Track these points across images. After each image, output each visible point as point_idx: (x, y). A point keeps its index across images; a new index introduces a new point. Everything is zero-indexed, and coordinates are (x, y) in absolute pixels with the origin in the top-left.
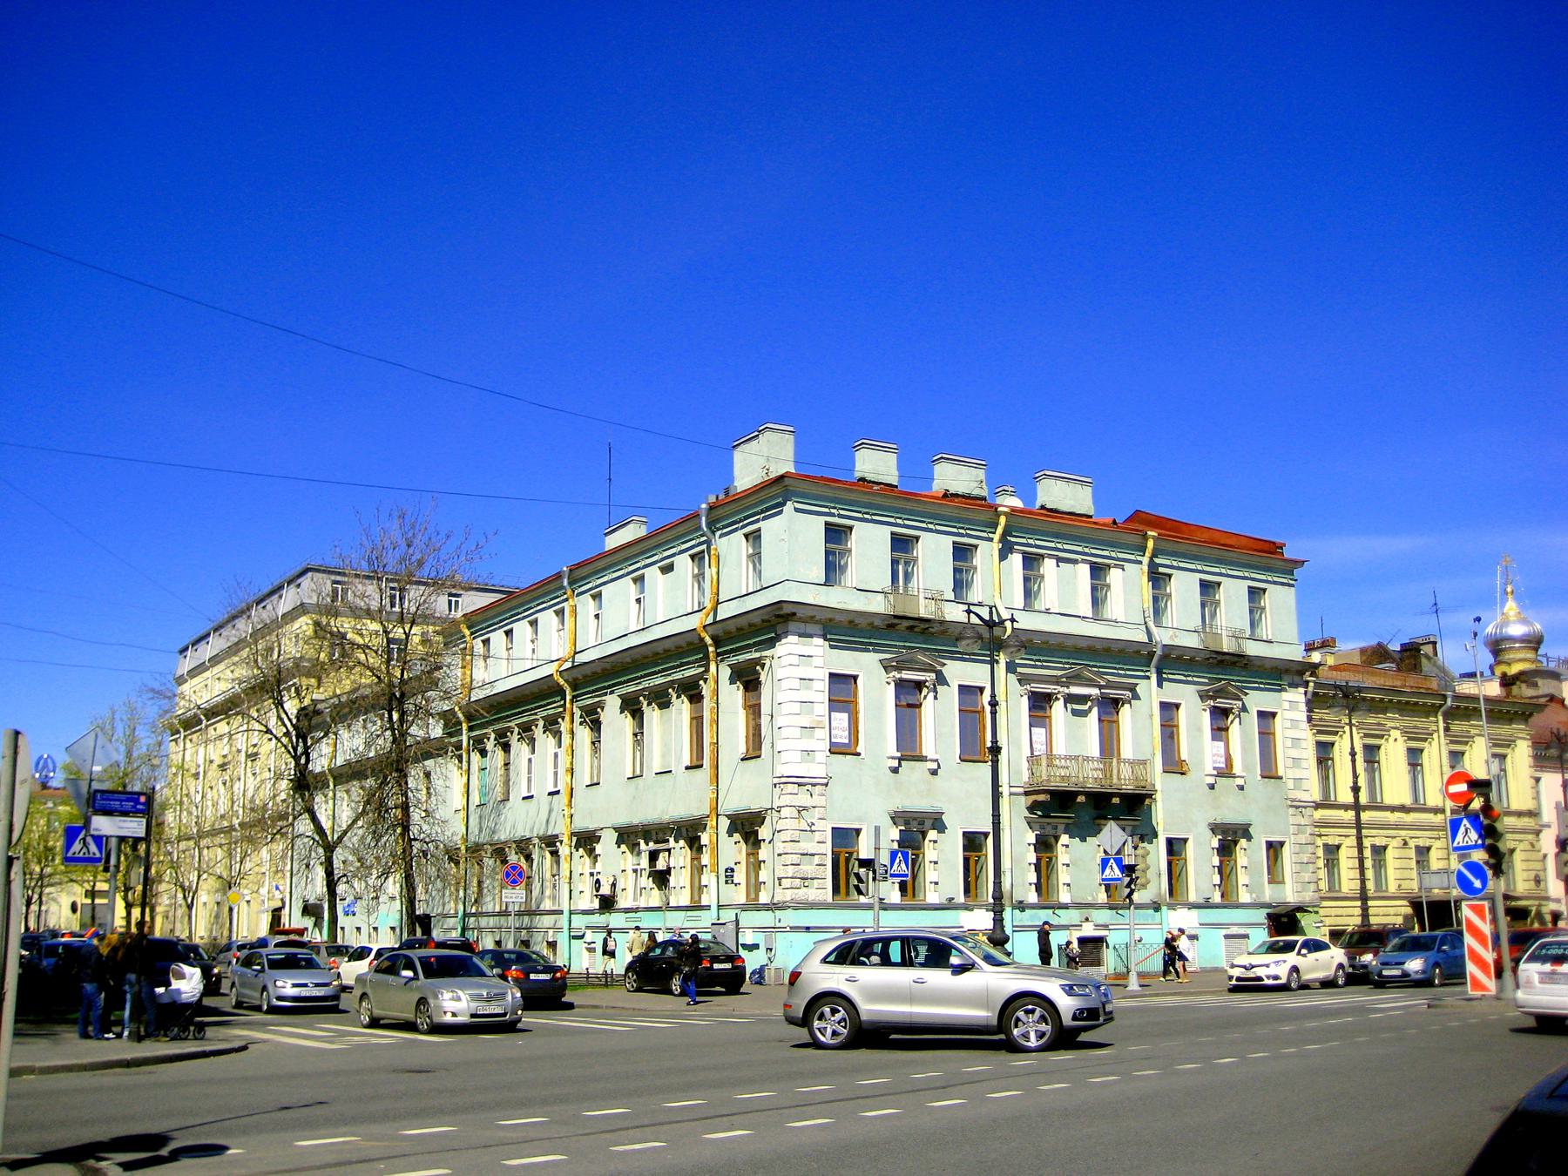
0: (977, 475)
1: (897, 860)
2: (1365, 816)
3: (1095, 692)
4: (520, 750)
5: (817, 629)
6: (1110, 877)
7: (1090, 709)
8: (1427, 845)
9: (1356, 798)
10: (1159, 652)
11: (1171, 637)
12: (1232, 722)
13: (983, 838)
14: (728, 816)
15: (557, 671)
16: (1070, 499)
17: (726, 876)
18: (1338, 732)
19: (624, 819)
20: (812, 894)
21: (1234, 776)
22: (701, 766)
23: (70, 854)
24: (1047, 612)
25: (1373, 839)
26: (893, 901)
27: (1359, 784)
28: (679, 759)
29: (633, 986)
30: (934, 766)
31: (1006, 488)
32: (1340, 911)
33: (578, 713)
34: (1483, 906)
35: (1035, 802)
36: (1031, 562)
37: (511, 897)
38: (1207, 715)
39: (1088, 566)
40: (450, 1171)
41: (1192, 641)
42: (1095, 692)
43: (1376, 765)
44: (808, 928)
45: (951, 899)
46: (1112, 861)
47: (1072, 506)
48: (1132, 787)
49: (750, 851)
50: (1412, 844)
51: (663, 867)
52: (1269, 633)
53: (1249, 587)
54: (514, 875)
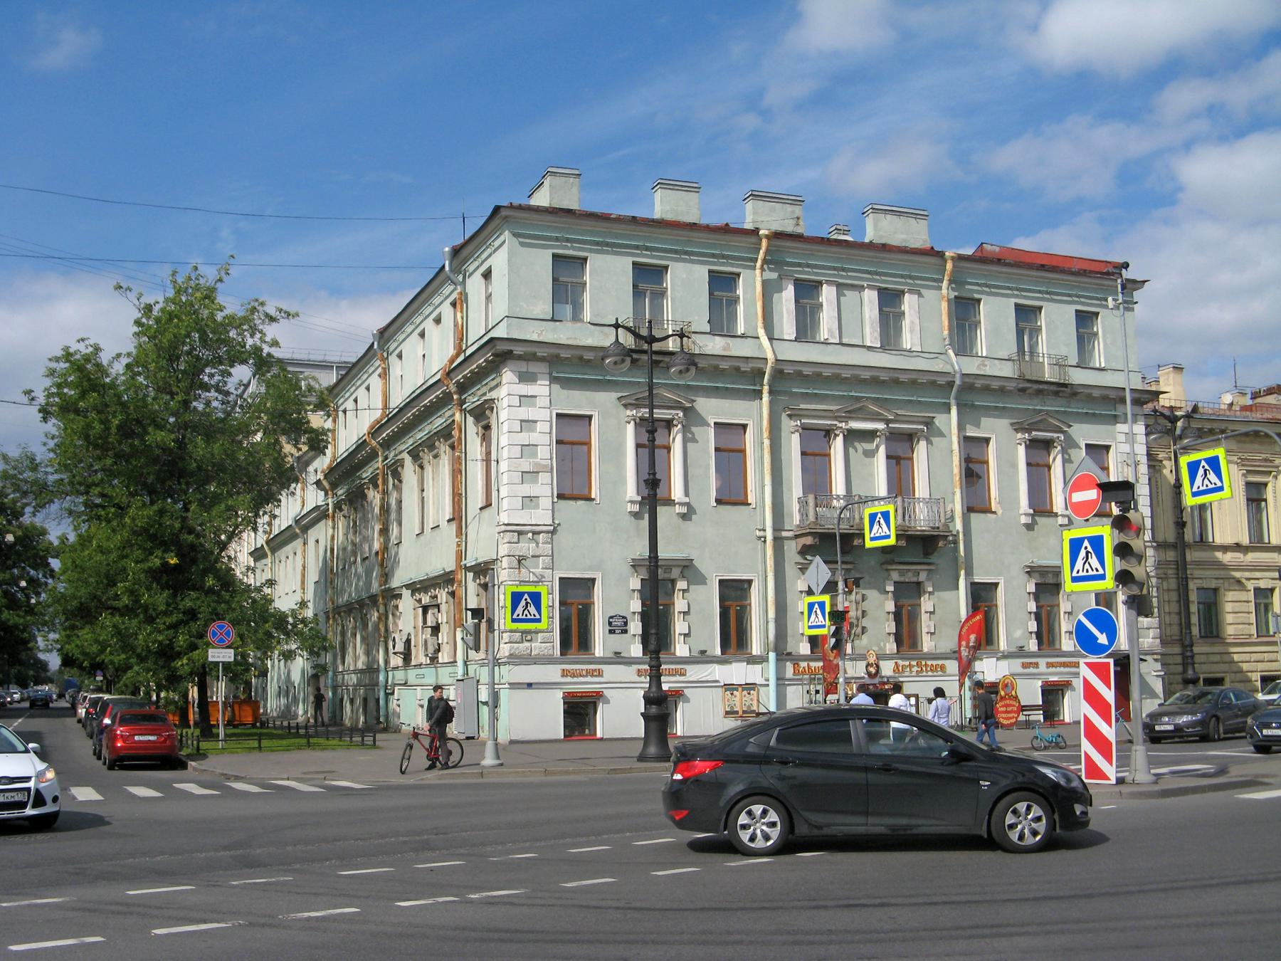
0: (793, 212)
2: (1191, 556)
3: (880, 426)
5: (542, 368)
6: (815, 624)
7: (878, 447)
8: (1213, 587)
9: (1181, 535)
10: (958, 382)
11: (978, 366)
12: (1054, 459)
13: (746, 586)
16: (902, 233)
18: (1271, 472)
20: (537, 647)
21: (1056, 515)
23: (515, 617)
24: (826, 343)
25: (1200, 581)
26: (802, 652)
27: (1184, 519)
28: (444, 516)
30: (684, 510)
31: (838, 227)
32: (1254, 657)
33: (390, 473)
34: (1109, 663)
35: (804, 546)
36: (807, 291)
37: (219, 657)
38: (1021, 450)
39: (876, 293)
40: (103, 939)
41: (1007, 370)
42: (880, 426)
43: (1263, 503)
44: (530, 685)
45: (703, 652)
47: (905, 241)
48: (927, 529)
50: (1250, 585)
51: (432, 622)
52: (1102, 360)
53: (1077, 311)
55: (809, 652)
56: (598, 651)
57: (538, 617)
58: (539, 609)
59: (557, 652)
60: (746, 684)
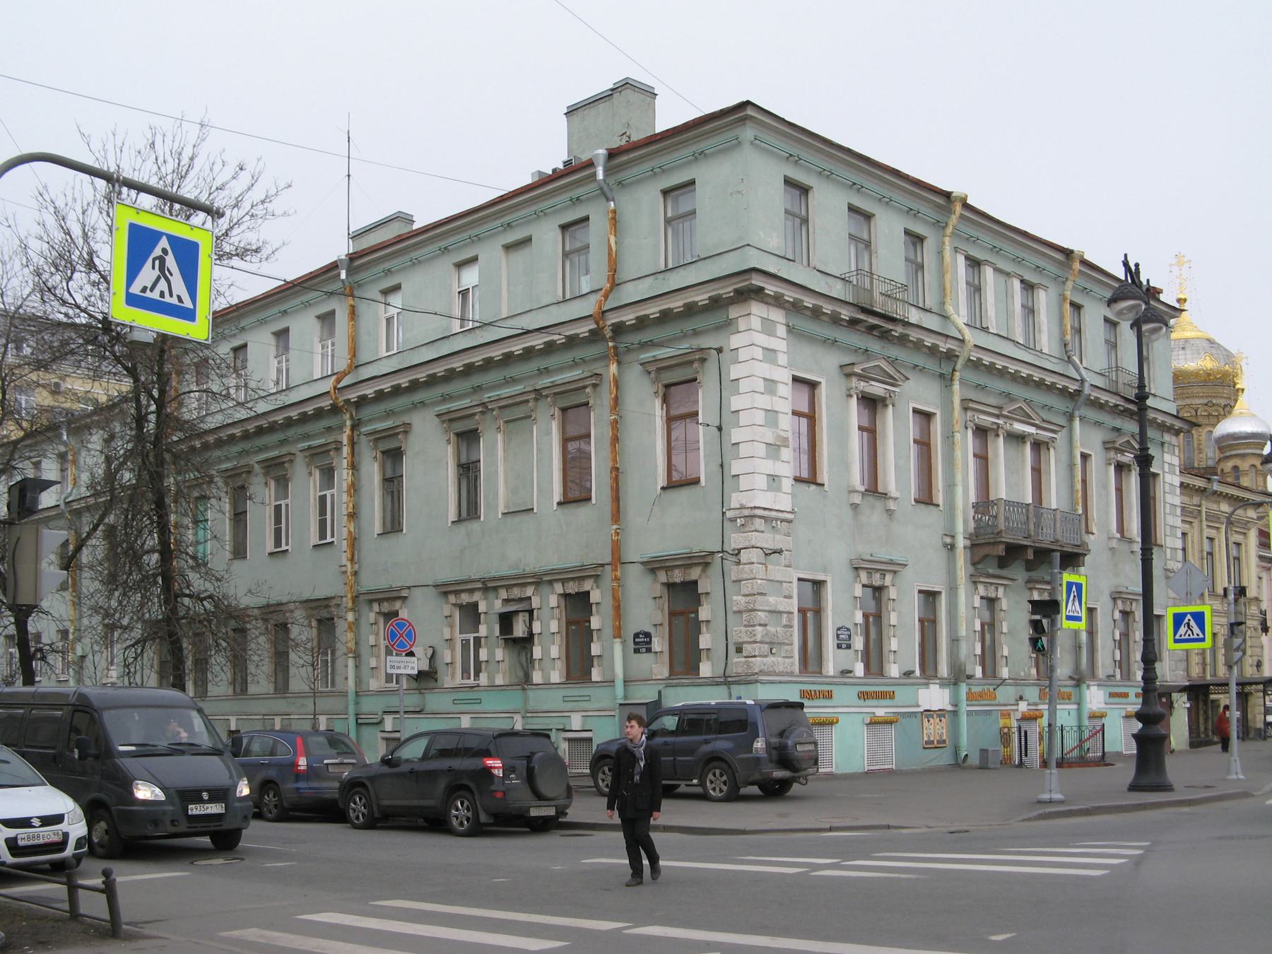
1: (1072, 595)
4: (263, 493)
14: (653, 566)
15: (335, 388)
17: (635, 643)
19: (447, 574)
22: (589, 499)
23: (1177, 637)
28: (545, 491)
29: (721, 791)
46: (1189, 617)
49: (680, 607)
51: (524, 633)
54: (401, 635)
55: (862, 675)
56: (830, 668)
57: (1201, 636)
58: (1202, 629)
59: (797, 670)
60: (940, 710)
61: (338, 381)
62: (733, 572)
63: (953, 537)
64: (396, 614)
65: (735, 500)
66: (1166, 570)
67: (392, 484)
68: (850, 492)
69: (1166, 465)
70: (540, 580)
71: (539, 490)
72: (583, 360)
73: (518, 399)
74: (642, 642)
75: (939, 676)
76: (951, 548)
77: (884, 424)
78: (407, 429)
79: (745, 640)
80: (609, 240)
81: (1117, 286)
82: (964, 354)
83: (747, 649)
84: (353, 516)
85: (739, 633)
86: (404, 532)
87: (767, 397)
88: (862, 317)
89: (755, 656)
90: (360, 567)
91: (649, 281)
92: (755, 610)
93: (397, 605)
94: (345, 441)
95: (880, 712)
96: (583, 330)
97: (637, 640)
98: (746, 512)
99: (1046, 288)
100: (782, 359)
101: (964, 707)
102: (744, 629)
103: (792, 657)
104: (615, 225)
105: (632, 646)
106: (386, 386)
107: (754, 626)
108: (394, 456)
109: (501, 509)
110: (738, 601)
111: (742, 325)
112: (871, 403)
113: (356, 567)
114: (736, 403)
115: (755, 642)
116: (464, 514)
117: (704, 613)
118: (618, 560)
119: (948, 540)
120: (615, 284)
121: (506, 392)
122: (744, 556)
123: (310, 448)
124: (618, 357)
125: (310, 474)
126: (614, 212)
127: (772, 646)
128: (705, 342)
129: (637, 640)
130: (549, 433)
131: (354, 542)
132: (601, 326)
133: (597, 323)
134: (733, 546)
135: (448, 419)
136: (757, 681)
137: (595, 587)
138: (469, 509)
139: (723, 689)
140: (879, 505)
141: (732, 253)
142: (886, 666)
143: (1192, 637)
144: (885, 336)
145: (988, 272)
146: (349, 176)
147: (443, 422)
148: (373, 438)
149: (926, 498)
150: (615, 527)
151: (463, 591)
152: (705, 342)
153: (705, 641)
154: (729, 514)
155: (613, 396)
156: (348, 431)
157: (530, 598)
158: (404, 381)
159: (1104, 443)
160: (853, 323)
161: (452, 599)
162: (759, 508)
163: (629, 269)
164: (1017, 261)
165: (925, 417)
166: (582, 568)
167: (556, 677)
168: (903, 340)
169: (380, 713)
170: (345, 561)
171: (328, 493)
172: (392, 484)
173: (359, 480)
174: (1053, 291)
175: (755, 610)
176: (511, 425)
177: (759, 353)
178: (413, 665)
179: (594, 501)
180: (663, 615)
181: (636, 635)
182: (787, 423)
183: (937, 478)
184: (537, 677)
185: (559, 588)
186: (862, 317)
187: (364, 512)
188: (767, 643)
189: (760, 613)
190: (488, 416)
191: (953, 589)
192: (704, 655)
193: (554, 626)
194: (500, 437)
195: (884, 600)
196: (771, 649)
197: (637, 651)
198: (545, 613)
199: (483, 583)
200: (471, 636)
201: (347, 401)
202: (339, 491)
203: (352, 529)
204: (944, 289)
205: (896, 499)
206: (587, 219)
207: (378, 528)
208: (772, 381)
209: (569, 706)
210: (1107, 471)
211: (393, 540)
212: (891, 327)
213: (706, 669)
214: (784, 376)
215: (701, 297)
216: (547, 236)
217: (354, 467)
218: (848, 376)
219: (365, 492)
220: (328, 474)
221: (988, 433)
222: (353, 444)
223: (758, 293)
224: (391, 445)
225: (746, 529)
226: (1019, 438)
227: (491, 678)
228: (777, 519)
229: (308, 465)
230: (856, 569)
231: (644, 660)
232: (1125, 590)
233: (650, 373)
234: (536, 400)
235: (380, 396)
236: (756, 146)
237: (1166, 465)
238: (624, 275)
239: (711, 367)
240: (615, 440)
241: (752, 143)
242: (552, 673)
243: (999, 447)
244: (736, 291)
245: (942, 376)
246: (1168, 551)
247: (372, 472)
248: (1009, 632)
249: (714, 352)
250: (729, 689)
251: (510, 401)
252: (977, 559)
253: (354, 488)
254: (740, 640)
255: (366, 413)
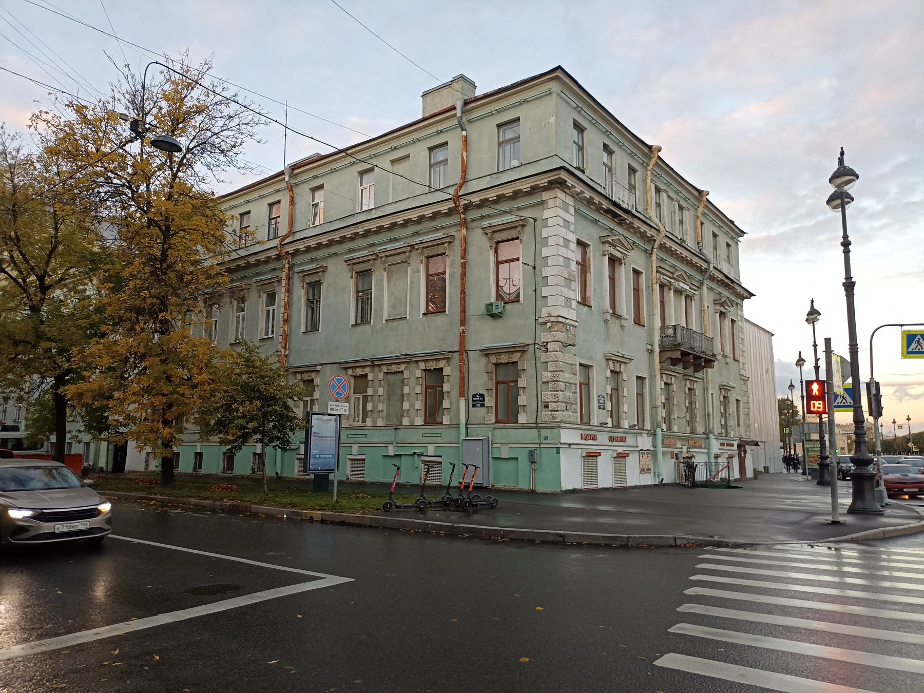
14: (487, 353)
15: (281, 244)
56: (595, 421)
60: (648, 450)
61: (283, 240)
62: (543, 357)
63: (652, 346)
64: (312, 380)
65: (544, 312)
66: (740, 375)
67: (313, 304)
68: (604, 313)
69: (739, 317)
70: (410, 359)
71: (411, 306)
72: (442, 228)
73: (398, 251)
74: (478, 400)
75: (645, 428)
76: (651, 352)
77: (619, 275)
78: (324, 270)
79: (551, 400)
80: (462, 154)
81: (102, 463)
82: (660, 239)
83: (552, 406)
84: (286, 321)
85: (547, 396)
86: (320, 331)
87: (565, 250)
88: (613, 208)
89: (558, 411)
90: (289, 352)
91: (488, 178)
92: (558, 381)
93: (313, 375)
94: (284, 276)
95: (620, 450)
96: (444, 208)
97: (474, 399)
98: (552, 319)
99: (689, 210)
100: (572, 228)
101: (660, 449)
102: (549, 393)
103: (576, 412)
104: (466, 145)
105: (471, 403)
106: (312, 243)
107: (558, 391)
108: (315, 286)
109: (385, 317)
110: (547, 376)
111: (551, 203)
112: (614, 261)
113: (287, 352)
114: (545, 252)
115: (558, 402)
116: (359, 321)
117: (522, 383)
118: (463, 351)
119: (650, 347)
120: (464, 181)
121: (389, 246)
122: (550, 346)
123: (260, 280)
124: (464, 223)
125: (260, 296)
126: (466, 137)
127: (568, 405)
128: (527, 214)
129: (474, 399)
130: (418, 271)
131: (286, 337)
132: (457, 205)
133: (455, 203)
134: (543, 340)
135: (351, 263)
136: (559, 427)
137: (446, 366)
138: (363, 317)
139: (535, 432)
140: (617, 322)
141: (544, 160)
142: (621, 420)
143: (846, 404)
144: (621, 222)
145: (664, 195)
146: (286, 135)
147: (349, 265)
148: (302, 275)
149: (638, 321)
150: (462, 328)
151: (358, 367)
152: (527, 214)
153: (522, 400)
154: (540, 320)
155: (463, 248)
156: (286, 270)
157: (402, 372)
158: (324, 240)
159: (714, 301)
160: (608, 211)
161: (350, 372)
162: (561, 316)
163: (472, 173)
164: (677, 192)
165: (637, 273)
166: (439, 353)
167: (419, 421)
168: (630, 227)
169: (298, 442)
170: (280, 347)
171: (271, 308)
172: (313, 304)
173: (292, 300)
174: (692, 212)
175: (558, 381)
176: (393, 267)
177: (561, 222)
178: (345, 408)
179: (447, 312)
180: (493, 384)
181: (474, 396)
182: (574, 267)
183: (643, 311)
184: (406, 421)
185: (422, 366)
186: (613, 208)
187: (294, 320)
188: (564, 403)
189: (561, 383)
190: (378, 261)
191: (653, 376)
192: (521, 409)
193: (418, 389)
194: (385, 274)
195: (620, 380)
196: (566, 407)
197: (474, 406)
198: (413, 381)
199: (372, 362)
200: (361, 396)
201: (287, 253)
202: (279, 307)
203: (286, 329)
204: (647, 201)
205: (626, 319)
206: (446, 143)
207: (303, 329)
208: (567, 240)
209: (427, 440)
210: (715, 316)
211: (312, 336)
212: (626, 217)
213: (522, 418)
214: (573, 238)
215: (525, 186)
216: (420, 153)
217: (289, 291)
218: (603, 243)
219: (295, 307)
220: (271, 298)
221: (664, 288)
222: (289, 278)
223: (561, 184)
224: (314, 279)
225: (553, 330)
226: (678, 292)
227: (374, 421)
228: (570, 325)
229: (259, 291)
230: (608, 359)
231: (479, 412)
232: (727, 384)
233: (487, 234)
234: (411, 251)
235: (309, 249)
236: (561, 97)
237: (739, 317)
238: (470, 176)
239: (529, 230)
240: (464, 275)
241: (558, 95)
242: (416, 419)
243: (671, 296)
244: (549, 182)
245: (646, 250)
246: (741, 364)
247: (300, 295)
248: (677, 405)
249: (532, 220)
250: (539, 431)
251: (394, 252)
252: (663, 359)
253: (288, 305)
254: (547, 400)
255: (299, 259)
